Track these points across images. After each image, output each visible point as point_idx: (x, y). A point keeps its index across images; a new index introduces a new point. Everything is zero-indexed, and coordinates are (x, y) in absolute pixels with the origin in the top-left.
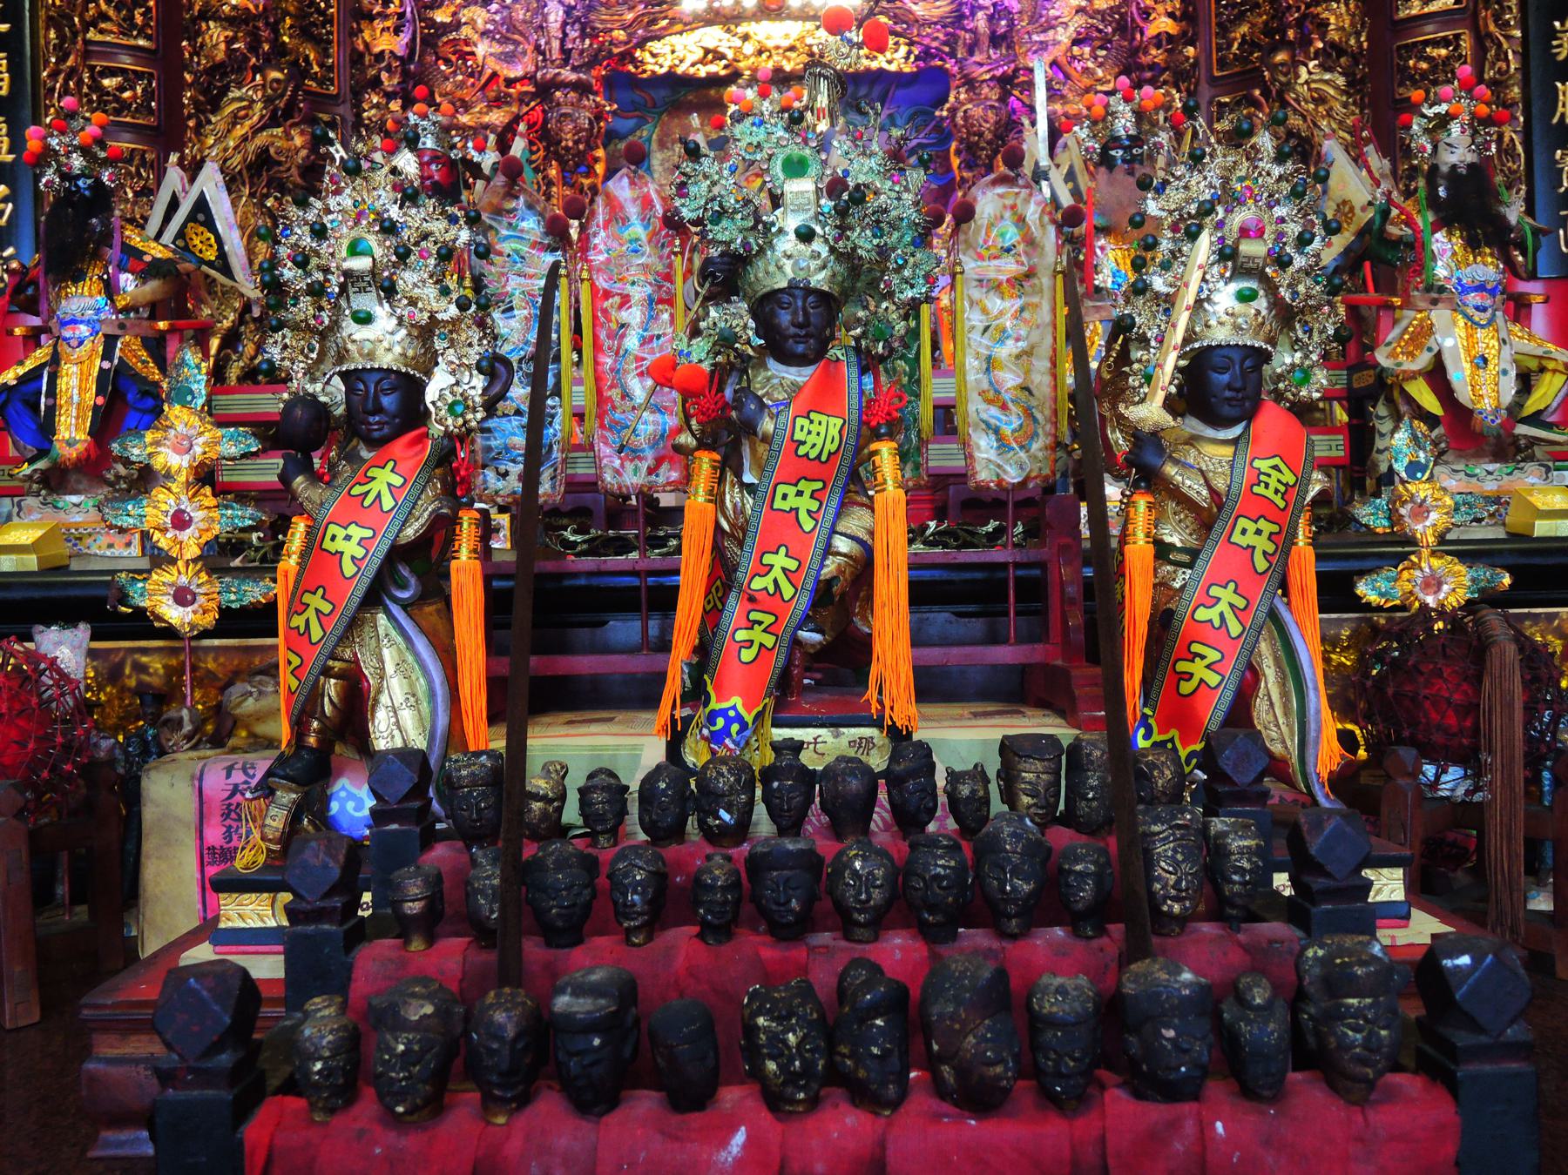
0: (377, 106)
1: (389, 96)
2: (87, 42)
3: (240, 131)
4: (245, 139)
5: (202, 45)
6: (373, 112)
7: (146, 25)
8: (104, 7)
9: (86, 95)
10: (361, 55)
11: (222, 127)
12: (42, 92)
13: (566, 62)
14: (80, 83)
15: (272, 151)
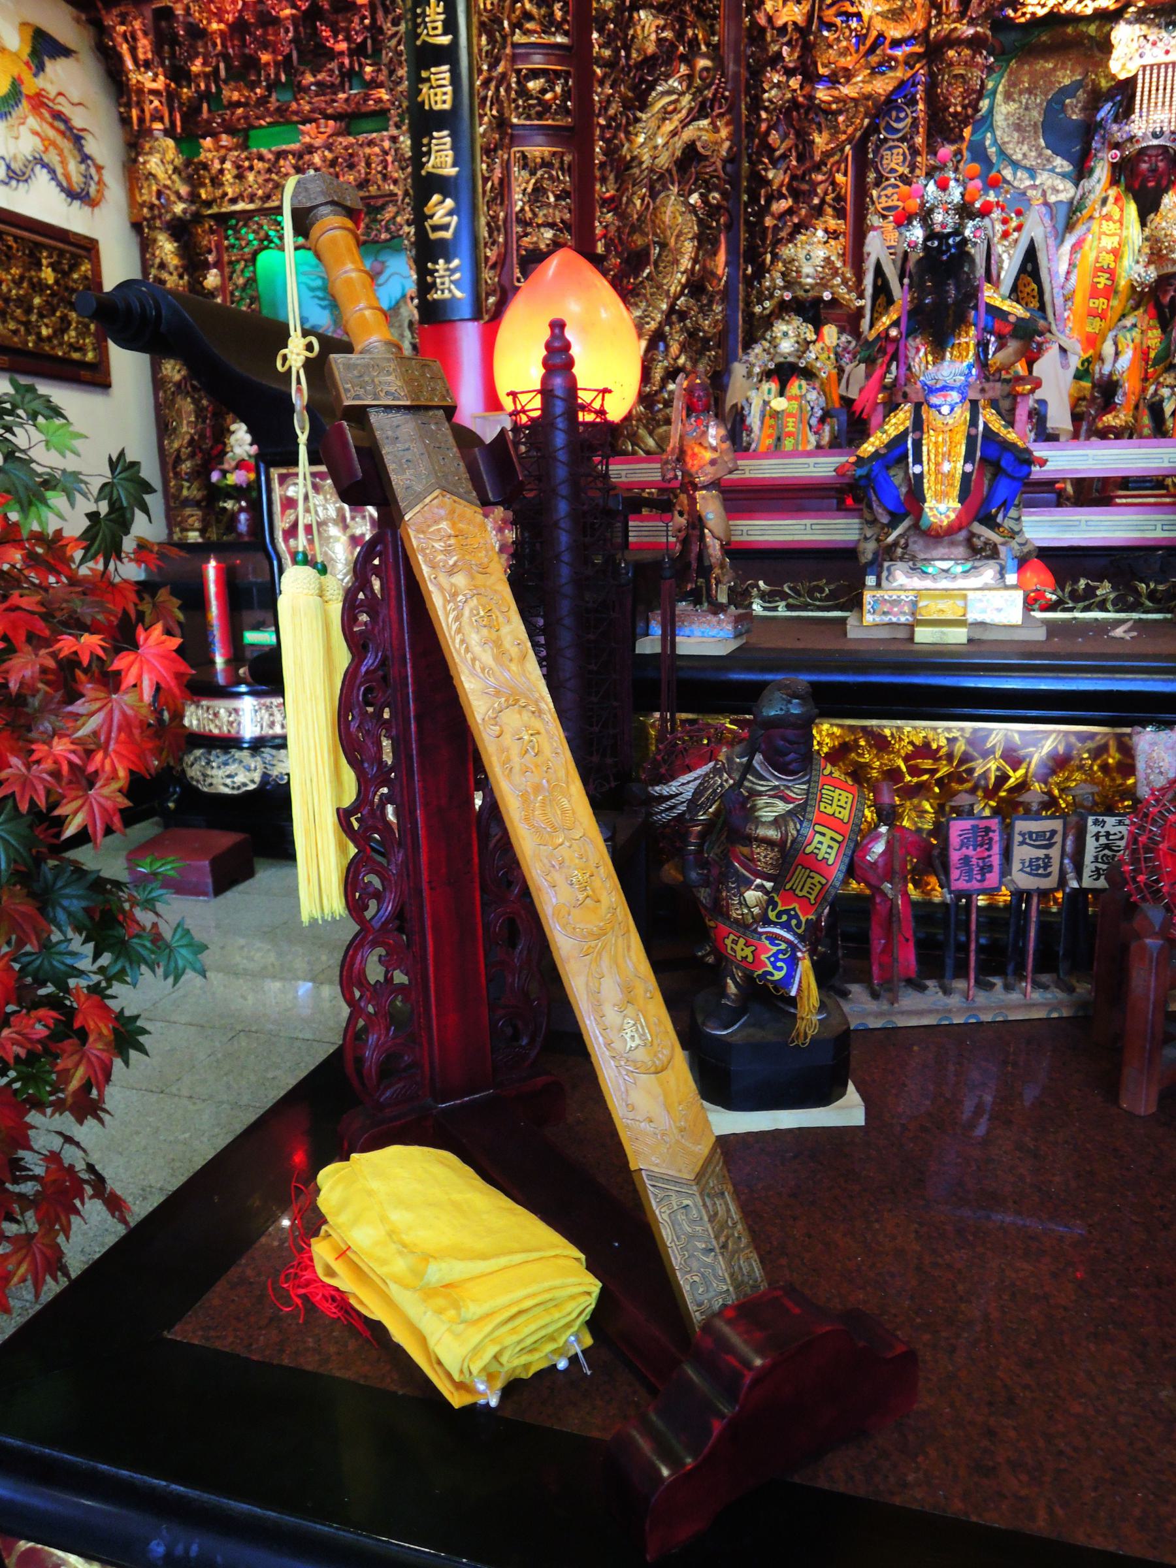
0: (778, 85)
1: (789, 73)
2: (515, 45)
3: (669, 127)
4: (674, 133)
5: (633, 37)
6: (773, 92)
7: (564, 20)
8: (528, 6)
9: (515, 101)
10: (763, 30)
11: (653, 124)
12: (477, 101)
13: (962, 14)
14: (508, 89)
15: (699, 144)
